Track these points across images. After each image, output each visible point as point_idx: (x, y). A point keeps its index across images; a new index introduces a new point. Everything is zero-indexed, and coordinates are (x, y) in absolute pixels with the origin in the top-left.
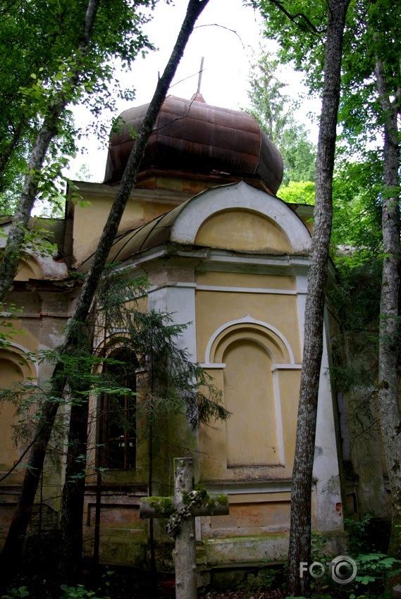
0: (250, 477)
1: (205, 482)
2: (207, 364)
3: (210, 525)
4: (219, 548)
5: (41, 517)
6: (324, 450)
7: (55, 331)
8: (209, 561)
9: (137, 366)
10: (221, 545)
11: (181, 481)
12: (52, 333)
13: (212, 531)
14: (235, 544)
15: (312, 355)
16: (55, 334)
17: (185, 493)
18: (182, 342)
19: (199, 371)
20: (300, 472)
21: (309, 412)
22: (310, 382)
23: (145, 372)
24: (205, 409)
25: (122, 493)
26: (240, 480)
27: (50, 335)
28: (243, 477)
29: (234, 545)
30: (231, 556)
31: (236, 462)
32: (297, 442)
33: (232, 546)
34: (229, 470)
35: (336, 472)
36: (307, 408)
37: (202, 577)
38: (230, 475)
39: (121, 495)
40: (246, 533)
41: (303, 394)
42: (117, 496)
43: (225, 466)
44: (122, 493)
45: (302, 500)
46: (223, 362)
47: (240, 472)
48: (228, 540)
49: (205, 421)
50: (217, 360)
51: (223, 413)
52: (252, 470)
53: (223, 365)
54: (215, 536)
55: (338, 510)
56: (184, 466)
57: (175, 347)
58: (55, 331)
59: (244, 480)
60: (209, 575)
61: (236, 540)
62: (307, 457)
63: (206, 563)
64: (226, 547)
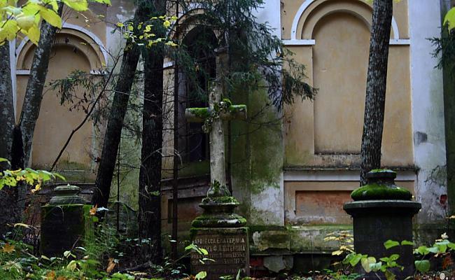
0: (340, 164)
1: (290, 167)
2: (294, 41)
3: (295, 212)
4: (304, 235)
5: (118, 216)
6: (429, 137)
7: (123, 11)
8: (293, 247)
9: (217, 46)
10: (306, 232)
11: (213, 96)
12: (120, 13)
13: (297, 218)
14: (321, 231)
15: (380, 19)
16: (123, 14)
17: (215, 104)
18: (264, 15)
19: (276, 44)
20: (367, 138)
21: (377, 78)
22: (377, 47)
23: (224, 52)
24: (293, 87)
25: (203, 184)
26: (329, 167)
27: (118, 15)
28: (333, 163)
29: (321, 233)
30: (316, 244)
31: (327, 150)
32: (366, 109)
33: (318, 233)
34: (316, 156)
35: (443, 162)
36: (374, 74)
37: (284, 261)
38: (318, 161)
39: (202, 186)
40: (334, 221)
41: (371, 60)
42: (199, 188)
43: (313, 151)
44: (203, 184)
45: (370, 165)
46: (313, 38)
47: (329, 158)
48: (314, 228)
49: (290, 102)
50: (305, 36)
51: (309, 92)
52: (343, 156)
53: (312, 42)
54: (300, 223)
55: (442, 202)
56: (215, 85)
57: (256, 21)
58: (123, 11)
59: (333, 167)
60: (292, 259)
61: (322, 228)
62: (375, 123)
63: (289, 248)
64: (311, 234)
